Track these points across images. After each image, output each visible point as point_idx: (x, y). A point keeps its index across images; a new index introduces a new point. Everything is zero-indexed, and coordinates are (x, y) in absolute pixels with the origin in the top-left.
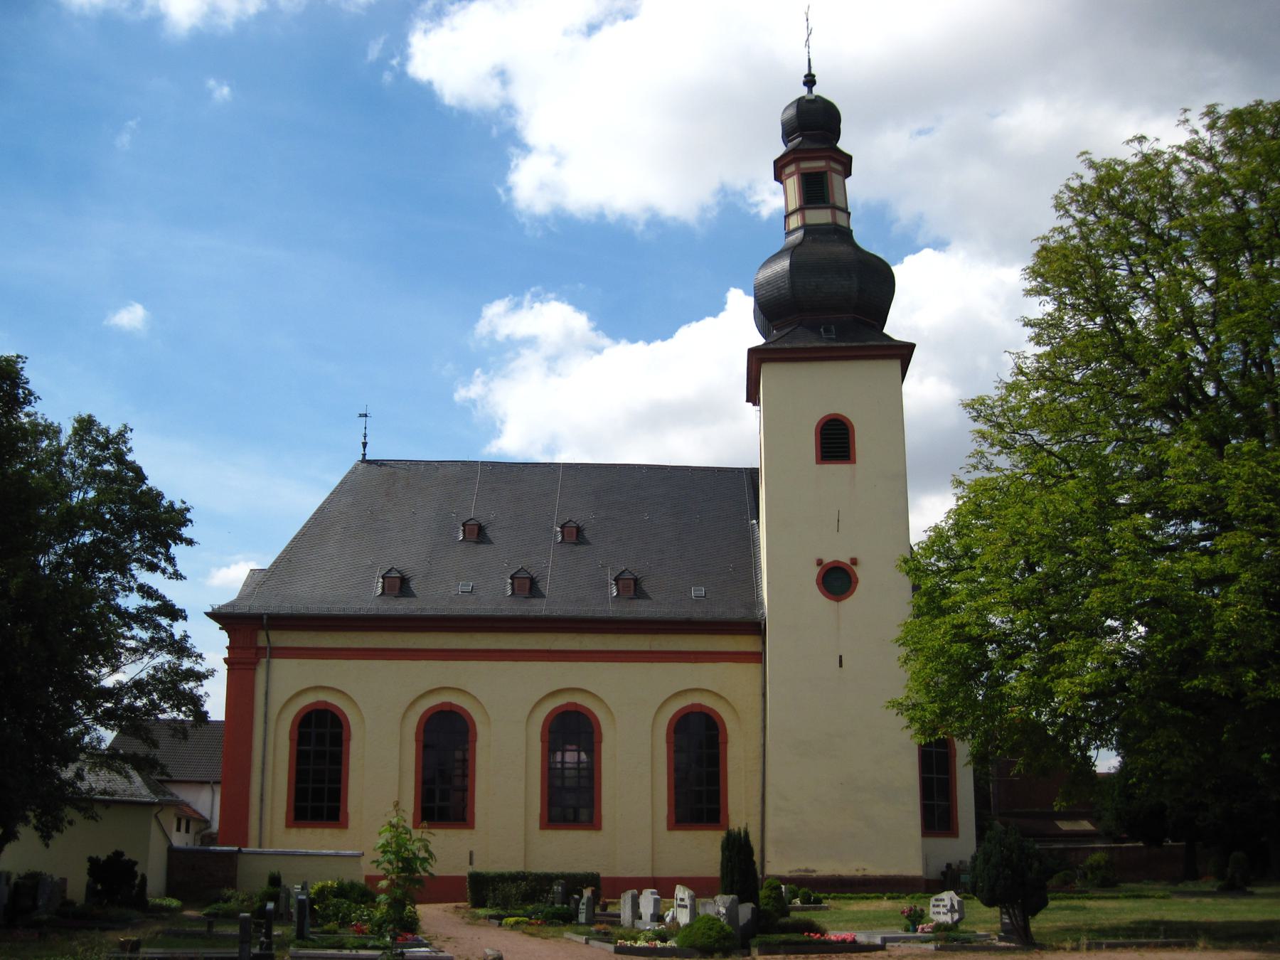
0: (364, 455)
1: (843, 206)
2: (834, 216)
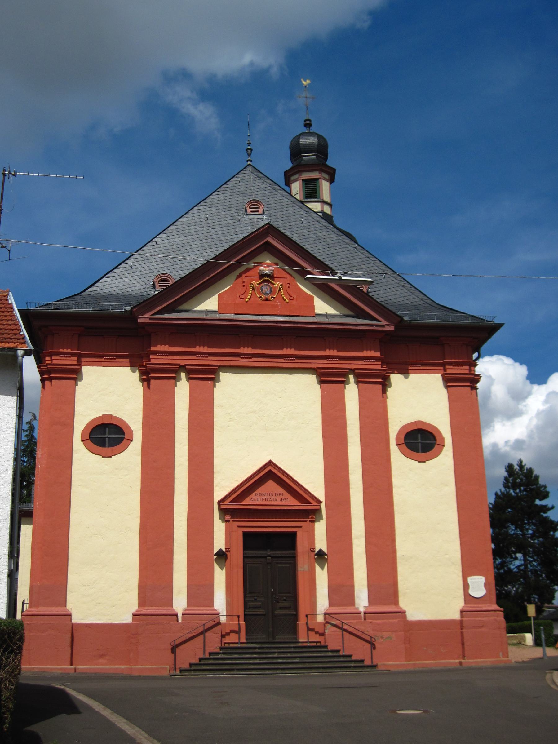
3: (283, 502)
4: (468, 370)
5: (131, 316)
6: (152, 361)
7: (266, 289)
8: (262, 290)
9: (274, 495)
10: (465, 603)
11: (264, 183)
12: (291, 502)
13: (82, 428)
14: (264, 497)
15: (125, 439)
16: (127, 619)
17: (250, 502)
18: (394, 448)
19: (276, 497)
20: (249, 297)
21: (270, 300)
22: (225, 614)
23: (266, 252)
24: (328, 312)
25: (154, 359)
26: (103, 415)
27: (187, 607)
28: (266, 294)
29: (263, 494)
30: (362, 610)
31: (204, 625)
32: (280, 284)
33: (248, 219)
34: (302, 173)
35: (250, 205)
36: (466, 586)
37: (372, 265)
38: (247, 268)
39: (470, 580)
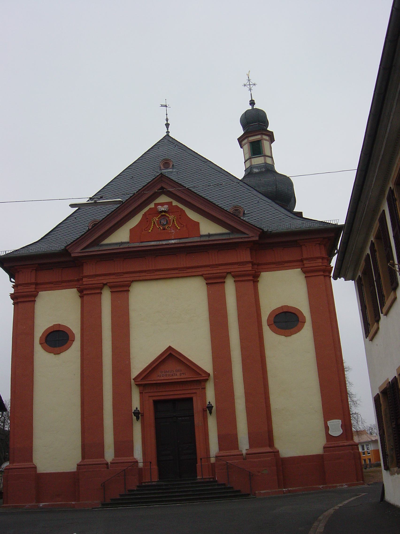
0: (168, 132)
1: (270, 155)
2: (265, 159)
4: (321, 263)
5: (65, 252)
6: (85, 283)
7: (164, 222)
8: (161, 222)
9: (175, 371)
10: (327, 441)
12: (187, 376)
13: (40, 335)
15: (69, 341)
18: (266, 329)
19: (177, 373)
20: (151, 229)
21: (166, 229)
24: (210, 233)
26: (54, 325)
27: (114, 457)
28: (164, 225)
29: (167, 371)
30: (244, 452)
31: (125, 470)
34: (249, 138)
36: (327, 428)
37: (250, 194)
38: (150, 208)
39: (330, 423)
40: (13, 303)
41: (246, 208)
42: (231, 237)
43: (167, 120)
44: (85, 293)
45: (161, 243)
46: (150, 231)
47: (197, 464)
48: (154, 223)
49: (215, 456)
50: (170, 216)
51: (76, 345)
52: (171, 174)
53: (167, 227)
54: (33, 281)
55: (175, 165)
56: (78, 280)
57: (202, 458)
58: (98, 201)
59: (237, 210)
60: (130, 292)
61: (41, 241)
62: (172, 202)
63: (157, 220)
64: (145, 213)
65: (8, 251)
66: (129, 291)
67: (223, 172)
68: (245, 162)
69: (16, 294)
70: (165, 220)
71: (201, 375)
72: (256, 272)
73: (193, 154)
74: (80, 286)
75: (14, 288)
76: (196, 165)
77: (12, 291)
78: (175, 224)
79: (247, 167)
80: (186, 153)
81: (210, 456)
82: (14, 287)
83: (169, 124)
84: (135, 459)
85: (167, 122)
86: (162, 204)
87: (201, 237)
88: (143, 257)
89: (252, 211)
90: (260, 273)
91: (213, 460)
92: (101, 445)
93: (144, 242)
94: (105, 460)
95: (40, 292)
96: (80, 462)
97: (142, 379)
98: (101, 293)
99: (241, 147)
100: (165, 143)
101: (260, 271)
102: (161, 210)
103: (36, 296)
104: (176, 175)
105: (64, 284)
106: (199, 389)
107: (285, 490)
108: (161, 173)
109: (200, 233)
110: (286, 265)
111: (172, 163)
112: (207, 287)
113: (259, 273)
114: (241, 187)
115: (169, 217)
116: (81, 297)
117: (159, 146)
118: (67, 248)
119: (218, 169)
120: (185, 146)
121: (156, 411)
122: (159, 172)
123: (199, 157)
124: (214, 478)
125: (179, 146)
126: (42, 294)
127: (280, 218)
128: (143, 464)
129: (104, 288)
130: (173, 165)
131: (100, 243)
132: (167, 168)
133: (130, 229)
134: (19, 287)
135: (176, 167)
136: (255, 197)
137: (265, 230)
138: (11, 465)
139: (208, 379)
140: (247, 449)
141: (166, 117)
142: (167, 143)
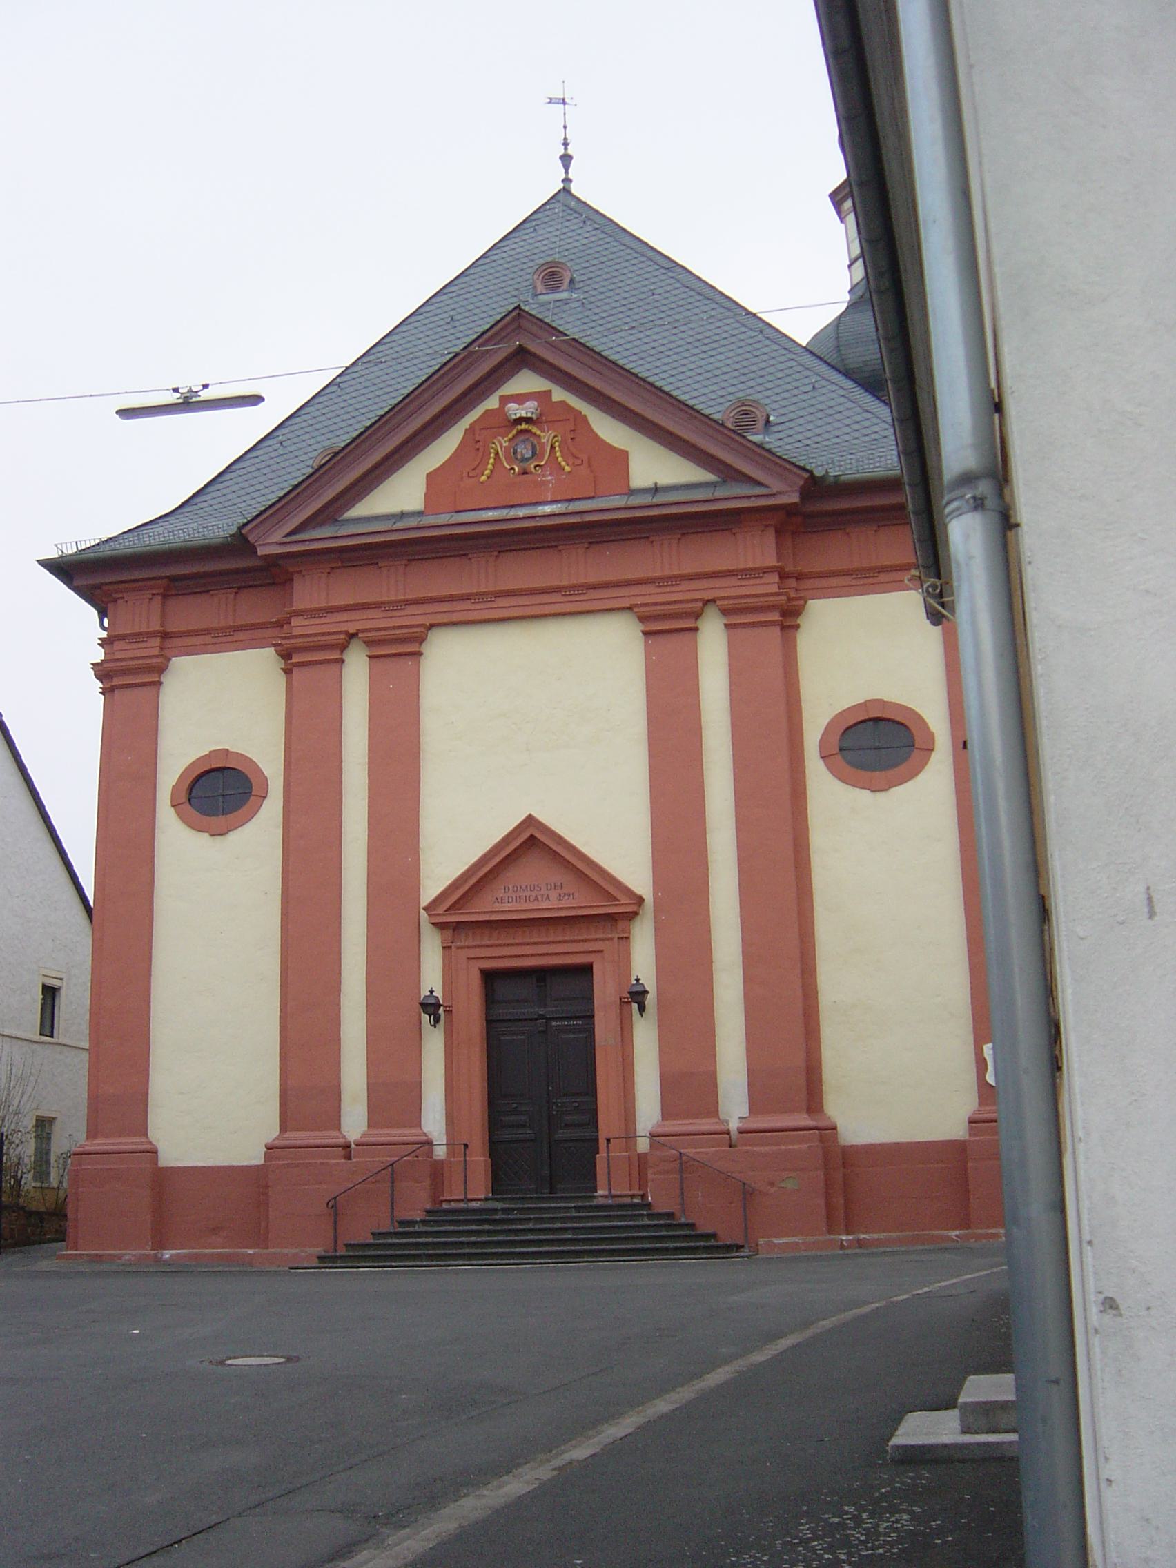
0: (567, 180)
3: (563, 902)
5: (240, 543)
6: (296, 632)
8: (515, 452)
9: (544, 888)
10: (980, 1104)
11: (588, 223)
12: (580, 902)
14: (523, 894)
15: (252, 798)
16: (250, 1153)
17: (492, 906)
18: (815, 769)
20: (487, 472)
21: (531, 473)
22: (445, 1142)
23: (525, 370)
25: (299, 625)
27: (366, 1129)
28: (524, 460)
30: (734, 1125)
31: (392, 1165)
32: (553, 435)
33: (537, 306)
35: (543, 274)
38: (487, 411)
40: (101, 690)
41: (774, 406)
42: (720, 493)
43: (566, 144)
44: (297, 661)
45: (513, 513)
46: (483, 478)
47: (598, 1155)
48: (497, 454)
49: (648, 1135)
50: (542, 434)
51: (271, 810)
52: (567, 307)
53: (532, 466)
54: (157, 627)
55: (578, 279)
56: (280, 624)
57: (611, 1137)
58: (194, 400)
59: (746, 413)
60: (423, 657)
61: (180, 511)
62: (550, 392)
63: (505, 447)
64: (471, 425)
65: (83, 543)
66: (422, 654)
67: (717, 298)
68: (849, 266)
69: (109, 665)
70: (530, 448)
71: (616, 899)
72: (790, 599)
73: (634, 244)
74: (283, 642)
75: (103, 647)
76: (640, 278)
77: (99, 655)
78: (557, 458)
79: (855, 282)
80: (615, 244)
81: (635, 1132)
82: (104, 643)
83: (570, 157)
84: (425, 1134)
85: (566, 149)
86: (520, 399)
87: (632, 495)
88: (519, 550)
89: (792, 416)
90: (806, 602)
91: (643, 1145)
92: (334, 1093)
93: (466, 511)
94: (341, 1133)
95: (173, 659)
96: (276, 1139)
97: (448, 909)
98: (342, 661)
99: (842, 220)
100: (556, 213)
101: (802, 595)
102: (515, 414)
103: (161, 669)
104: (579, 309)
105: (241, 636)
106: (611, 939)
107: (847, 1241)
108: (518, 307)
109: (631, 484)
110: (883, 577)
111: (569, 274)
112: (646, 642)
113: (802, 602)
114: (767, 342)
115: (539, 436)
116: (287, 671)
117: (538, 222)
118: (244, 531)
119: (706, 291)
120: (614, 222)
121: (490, 999)
122: (531, 301)
123: (650, 253)
124: (643, 1196)
125: (595, 223)
126: (181, 664)
127: (875, 436)
128: (445, 1150)
129: (350, 646)
130: (572, 281)
131: (341, 516)
132: (553, 289)
133: (428, 472)
134: (118, 645)
135: (581, 285)
136: (807, 373)
137: (818, 472)
138: (89, 1143)
139: (636, 914)
140: (741, 1116)
141: (563, 137)
142: (561, 215)
